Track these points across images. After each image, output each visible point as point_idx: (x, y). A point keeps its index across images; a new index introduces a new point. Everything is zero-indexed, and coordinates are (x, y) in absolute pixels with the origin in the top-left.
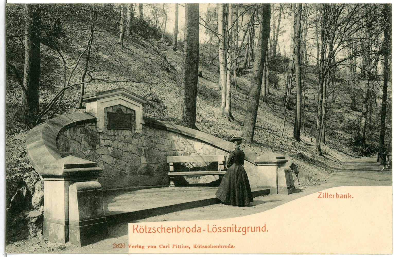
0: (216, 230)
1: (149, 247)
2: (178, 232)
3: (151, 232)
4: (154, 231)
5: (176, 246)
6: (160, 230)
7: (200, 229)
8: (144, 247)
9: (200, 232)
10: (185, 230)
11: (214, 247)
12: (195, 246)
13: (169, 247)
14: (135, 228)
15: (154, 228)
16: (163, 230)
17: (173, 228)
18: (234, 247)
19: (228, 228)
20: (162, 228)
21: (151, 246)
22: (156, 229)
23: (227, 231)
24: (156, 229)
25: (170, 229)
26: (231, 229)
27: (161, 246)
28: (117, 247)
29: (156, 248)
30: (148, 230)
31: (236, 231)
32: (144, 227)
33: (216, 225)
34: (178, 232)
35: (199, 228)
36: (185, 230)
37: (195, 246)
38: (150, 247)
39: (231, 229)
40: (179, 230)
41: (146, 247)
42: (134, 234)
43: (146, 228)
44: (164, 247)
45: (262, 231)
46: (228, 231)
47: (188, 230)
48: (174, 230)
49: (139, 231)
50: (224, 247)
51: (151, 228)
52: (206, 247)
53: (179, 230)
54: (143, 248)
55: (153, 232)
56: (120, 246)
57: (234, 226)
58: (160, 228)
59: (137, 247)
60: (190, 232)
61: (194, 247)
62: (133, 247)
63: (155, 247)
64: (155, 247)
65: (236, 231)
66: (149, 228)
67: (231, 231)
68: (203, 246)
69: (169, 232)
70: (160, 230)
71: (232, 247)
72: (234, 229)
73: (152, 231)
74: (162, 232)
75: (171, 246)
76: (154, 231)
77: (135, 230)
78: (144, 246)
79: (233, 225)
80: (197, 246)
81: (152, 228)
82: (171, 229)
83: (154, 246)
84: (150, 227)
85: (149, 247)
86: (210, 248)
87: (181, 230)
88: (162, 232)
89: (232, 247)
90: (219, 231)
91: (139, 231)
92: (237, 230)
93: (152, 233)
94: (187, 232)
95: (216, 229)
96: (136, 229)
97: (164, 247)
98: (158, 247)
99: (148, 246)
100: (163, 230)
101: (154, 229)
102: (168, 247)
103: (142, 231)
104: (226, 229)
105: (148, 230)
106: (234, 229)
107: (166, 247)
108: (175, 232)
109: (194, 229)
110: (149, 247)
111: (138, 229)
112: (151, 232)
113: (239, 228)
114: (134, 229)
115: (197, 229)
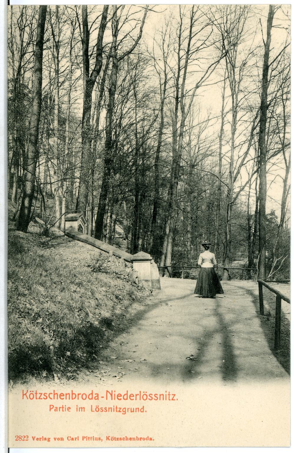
0: (82, 396)
1: (55, 439)
2: (72, 399)
3: (42, 399)
4: (45, 397)
5: (86, 439)
6: (52, 396)
7: (98, 396)
8: (50, 440)
9: (98, 399)
10: (80, 396)
11: (130, 439)
12: (108, 438)
13: (78, 440)
14: (24, 393)
15: (151, 394)
16: (56, 396)
17: (66, 394)
18: (154, 440)
19: (160, 395)
20: (54, 394)
21: (57, 438)
22: (47, 395)
23: (159, 399)
24: (47, 395)
25: (134, 396)
26: (69, 396)
27: (69, 438)
28: (20, 439)
29: (63, 440)
30: (38, 396)
31: (169, 400)
32: (34, 393)
33: (166, 392)
34: (72, 399)
35: (97, 395)
36: (80, 396)
37: (108, 438)
38: (57, 439)
39: (69, 396)
40: (74, 396)
41: (52, 440)
42: (91, 404)
43: (36, 394)
44: (73, 439)
45: (143, 399)
46: (160, 399)
47: (84, 397)
48: (68, 396)
49: (28, 397)
50: (142, 439)
51: (41, 394)
52: (121, 439)
53: (74, 396)
54: (49, 440)
55: (44, 398)
56: (22, 438)
57: (167, 393)
58: (52, 394)
59: (41, 440)
60: (33, 398)
61: (107, 440)
62: (37, 439)
63: (62, 439)
64: (62, 439)
65: (169, 400)
66: (172, 395)
67: (69, 399)
68: (118, 439)
69: (131, 400)
70: (52, 396)
71: (151, 439)
72: (168, 396)
73: (43, 396)
74: (54, 398)
75: (81, 438)
76: (45, 397)
77: (25, 396)
78: (50, 438)
79: (166, 392)
80: (110, 438)
81: (43, 393)
82: (135, 396)
83: (61, 438)
84: (174, 394)
85: (34, 439)
86: (125, 441)
87: (76, 397)
88: (54, 398)
89: (151, 439)
90: (151, 398)
91: (28, 397)
92: (171, 398)
93: (43, 399)
94: (83, 398)
95: (147, 396)
96: (26, 394)
97: (73, 439)
98: (65, 439)
99: (33, 437)
100: (56, 396)
101: (46, 395)
102: (77, 439)
103: (32, 396)
104: (158, 396)
105: (38, 396)
106: (168, 396)
107: (74, 439)
108: (69, 399)
109: (126, 396)
110: (34, 439)
111: (28, 395)
112: (42, 399)
113: (40, 395)
114: (23, 395)
115: (94, 396)
